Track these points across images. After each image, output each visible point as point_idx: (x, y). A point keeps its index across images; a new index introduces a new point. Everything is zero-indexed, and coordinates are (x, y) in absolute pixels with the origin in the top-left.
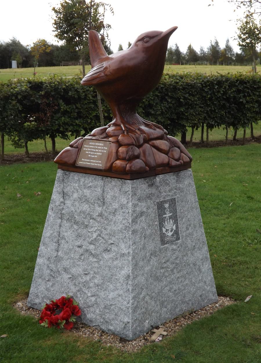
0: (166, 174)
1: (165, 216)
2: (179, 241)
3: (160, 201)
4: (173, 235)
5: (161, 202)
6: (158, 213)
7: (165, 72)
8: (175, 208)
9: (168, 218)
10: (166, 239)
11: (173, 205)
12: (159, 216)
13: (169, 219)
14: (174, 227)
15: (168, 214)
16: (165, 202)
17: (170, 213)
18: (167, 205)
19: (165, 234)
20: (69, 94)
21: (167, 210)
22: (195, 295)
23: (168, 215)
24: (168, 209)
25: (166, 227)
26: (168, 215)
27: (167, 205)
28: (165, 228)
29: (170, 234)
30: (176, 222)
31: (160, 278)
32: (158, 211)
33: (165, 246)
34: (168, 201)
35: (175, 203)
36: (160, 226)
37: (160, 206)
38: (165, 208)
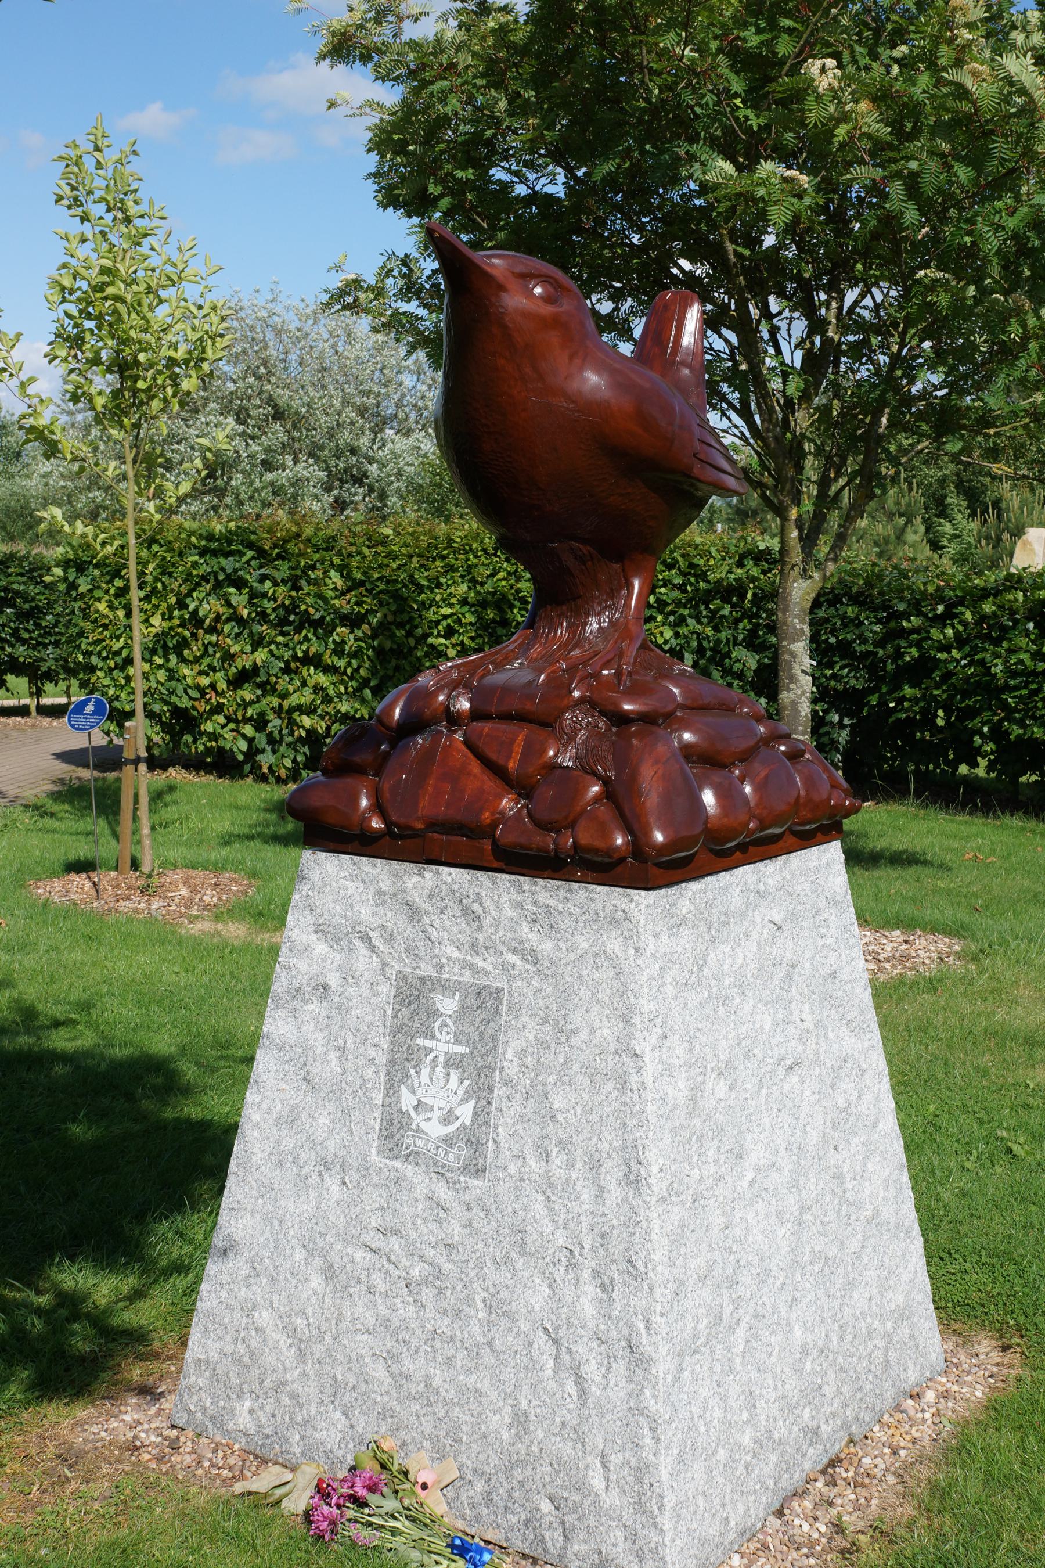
0: (479, 873)
1: (428, 1043)
2: (476, 1182)
3: (417, 971)
4: (448, 1141)
5: (423, 980)
6: (395, 1016)
7: (685, 536)
8: (490, 1031)
9: (441, 1059)
10: (410, 1141)
11: (481, 1015)
12: (398, 1030)
13: (447, 1065)
14: (466, 1113)
15: (448, 1042)
16: (447, 988)
17: (457, 1042)
18: (447, 1005)
19: (410, 1118)
20: (907, 52)
21: (444, 1025)
22: (518, 1474)
23: (443, 1045)
24: (449, 1022)
25: (420, 1092)
26: (445, 1048)
27: (447, 1005)
28: (413, 1092)
29: (435, 1129)
30: (481, 1091)
31: (343, 1277)
32: (396, 1012)
33: (398, 1164)
34: (457, 986)
35: (497, 1012)
36: (389, 1073)
37: (413, 999)
38: (435, 1014)
